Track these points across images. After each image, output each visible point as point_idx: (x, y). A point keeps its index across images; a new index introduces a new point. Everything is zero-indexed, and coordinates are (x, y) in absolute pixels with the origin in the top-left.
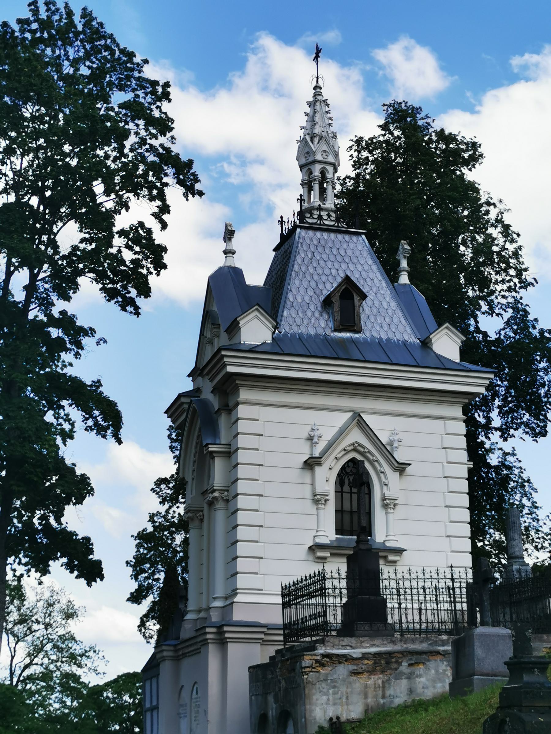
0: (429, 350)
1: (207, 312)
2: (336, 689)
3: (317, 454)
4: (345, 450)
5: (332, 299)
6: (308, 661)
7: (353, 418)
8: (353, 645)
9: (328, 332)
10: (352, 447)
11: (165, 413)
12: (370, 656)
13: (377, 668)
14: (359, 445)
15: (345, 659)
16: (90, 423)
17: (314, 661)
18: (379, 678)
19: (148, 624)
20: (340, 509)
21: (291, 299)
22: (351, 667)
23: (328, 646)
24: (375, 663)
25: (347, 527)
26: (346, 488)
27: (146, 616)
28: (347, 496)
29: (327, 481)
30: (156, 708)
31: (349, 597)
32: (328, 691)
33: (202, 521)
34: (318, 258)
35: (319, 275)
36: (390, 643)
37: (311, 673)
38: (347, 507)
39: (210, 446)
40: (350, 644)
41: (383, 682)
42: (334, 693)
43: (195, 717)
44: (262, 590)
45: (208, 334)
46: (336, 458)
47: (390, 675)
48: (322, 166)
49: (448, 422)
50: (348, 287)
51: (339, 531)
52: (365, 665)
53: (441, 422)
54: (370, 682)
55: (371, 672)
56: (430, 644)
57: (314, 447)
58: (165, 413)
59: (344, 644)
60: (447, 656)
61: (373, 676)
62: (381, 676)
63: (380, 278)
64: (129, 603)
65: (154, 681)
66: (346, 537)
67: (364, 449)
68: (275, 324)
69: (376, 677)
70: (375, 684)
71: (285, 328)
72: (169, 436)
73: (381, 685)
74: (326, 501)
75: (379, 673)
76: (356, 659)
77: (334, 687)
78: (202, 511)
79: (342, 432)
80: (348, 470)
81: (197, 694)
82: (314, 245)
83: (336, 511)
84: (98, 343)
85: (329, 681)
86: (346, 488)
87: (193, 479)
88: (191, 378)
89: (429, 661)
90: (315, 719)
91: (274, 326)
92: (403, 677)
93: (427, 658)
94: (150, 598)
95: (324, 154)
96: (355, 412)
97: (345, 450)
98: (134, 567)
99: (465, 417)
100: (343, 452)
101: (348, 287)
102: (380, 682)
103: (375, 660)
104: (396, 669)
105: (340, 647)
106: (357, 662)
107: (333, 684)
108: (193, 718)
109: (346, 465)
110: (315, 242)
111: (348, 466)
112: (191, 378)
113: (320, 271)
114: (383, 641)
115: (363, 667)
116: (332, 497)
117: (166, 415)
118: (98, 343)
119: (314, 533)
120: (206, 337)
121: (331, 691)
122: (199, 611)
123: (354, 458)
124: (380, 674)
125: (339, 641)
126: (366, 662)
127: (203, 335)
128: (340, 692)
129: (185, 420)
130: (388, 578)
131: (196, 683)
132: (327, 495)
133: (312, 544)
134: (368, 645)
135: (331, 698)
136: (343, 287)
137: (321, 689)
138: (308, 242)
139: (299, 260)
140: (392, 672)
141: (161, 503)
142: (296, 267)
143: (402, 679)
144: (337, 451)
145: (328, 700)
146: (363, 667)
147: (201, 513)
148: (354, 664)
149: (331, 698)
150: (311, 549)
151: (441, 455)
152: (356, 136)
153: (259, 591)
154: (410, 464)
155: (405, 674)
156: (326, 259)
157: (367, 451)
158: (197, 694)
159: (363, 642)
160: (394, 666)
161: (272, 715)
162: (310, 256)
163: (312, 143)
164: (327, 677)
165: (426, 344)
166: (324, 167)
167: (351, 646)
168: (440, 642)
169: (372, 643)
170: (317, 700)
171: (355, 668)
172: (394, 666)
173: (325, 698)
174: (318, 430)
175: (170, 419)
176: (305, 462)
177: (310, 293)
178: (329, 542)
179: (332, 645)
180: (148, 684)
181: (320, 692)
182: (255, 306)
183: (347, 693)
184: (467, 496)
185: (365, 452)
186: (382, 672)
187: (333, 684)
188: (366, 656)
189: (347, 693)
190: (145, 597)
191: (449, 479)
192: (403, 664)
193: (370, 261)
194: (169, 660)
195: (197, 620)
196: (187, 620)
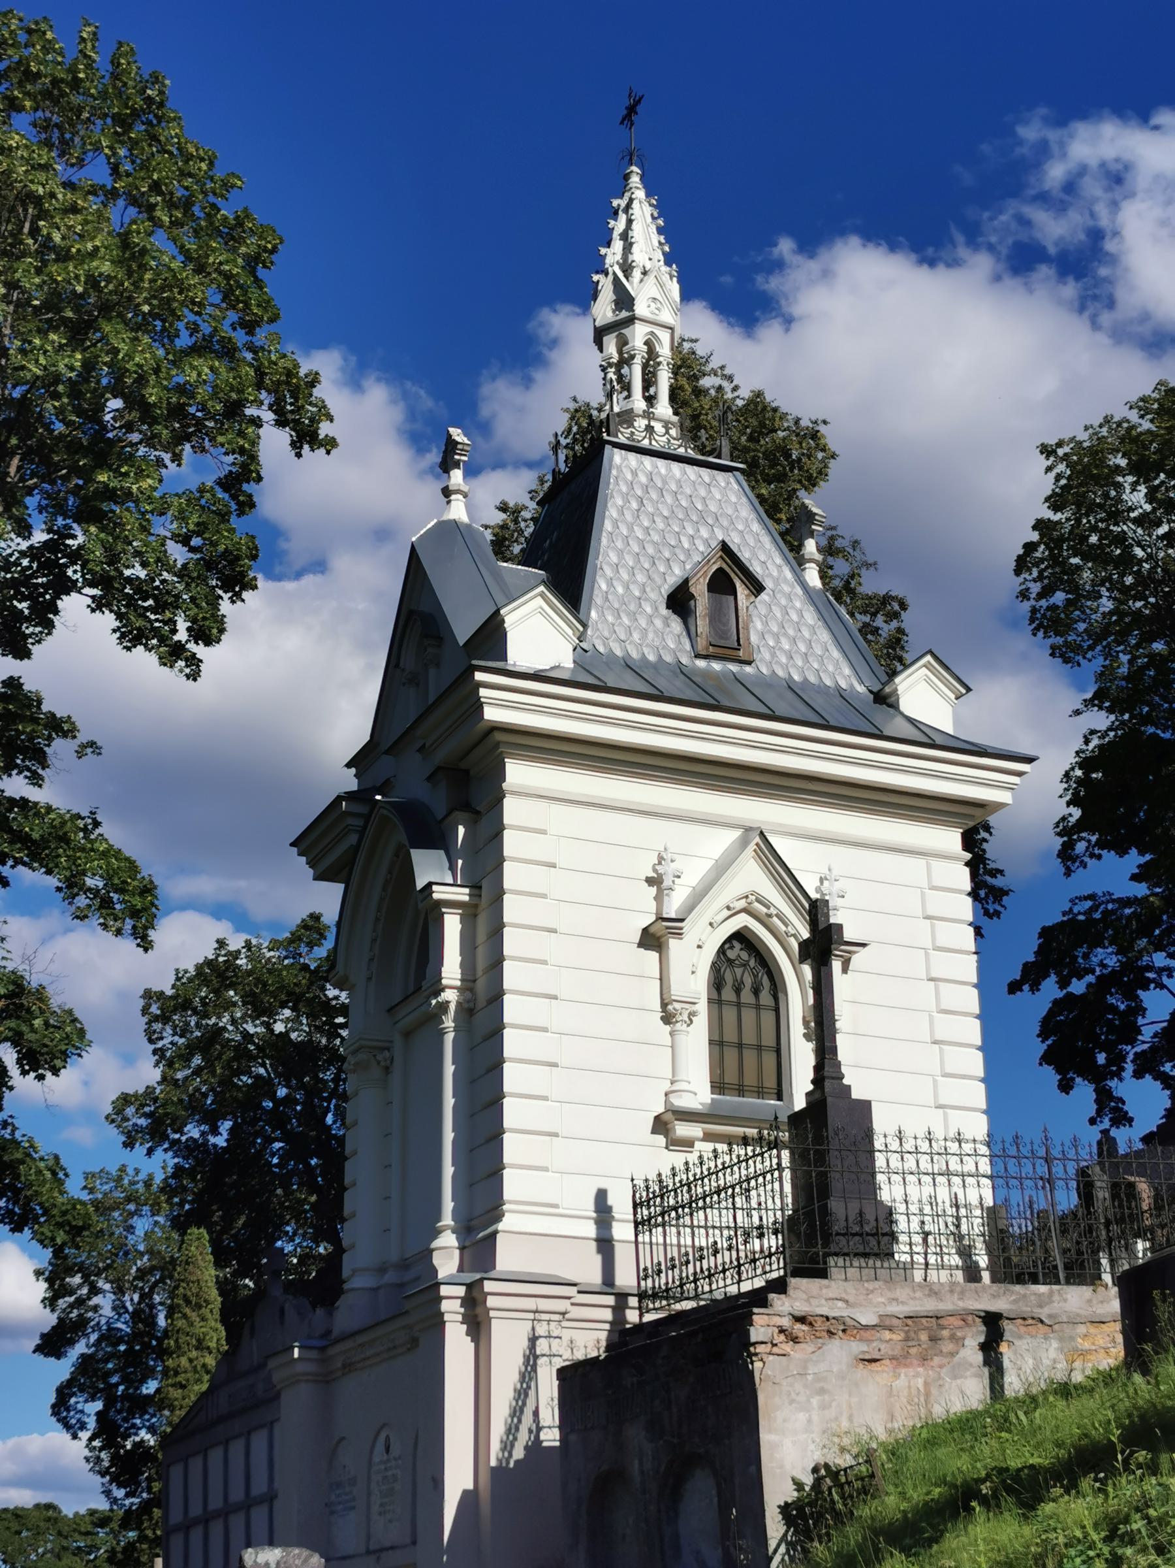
0: (891, 711)
1: (411, 613)
2: (826, 1397)
3: (671, 911)
4: (728, 908)
5: (692, 590)
6: (762, 1330)
7: (744, 843)
8: (851, 1299)
9: (685, 660)
10: (742, 904)
11: (292, 845)
12: (896, 1322)
13: (913, 1351)
14: (758, 900)
15: (842, 1327)
16: (82, 901)
17: (777, 1330)
18: (917, 1375)
19: (73, 1400)
20: (716, 1038)
21: (604, 587)
22: (857, 1347)
23: (796, 1299)
24: (907, 1339)
25: (731, 1077)
26: (728, 994)
27: (69, 1383)
28: (730, 1014)
29: (693, 972)
30: (270, 1498)
31: (793, 1210)
32: (809, 1401)
33: (387, 1070)
34: (651, 509)
35: (655, 543)
36: (929, 1296)
37: (771, 1358)
38: (730, 1035)
39: (435, 888)
40: (844, 1296)
41: (926, 1384)
42: (823, 1407)
43: (382, 1505)
44: (556, 1206)
45: (409, 661)
46: (711, 924)
47: (941, 1367)
48: (650, 330)
49: (936, 864)
50: (725, 566)
51: (718, 1086)
52: (887, 1342)
53: (921, 862)
54: (901, 1383)
55: (902, 1360)
56: (1015, 1302)
57: (666, 898)
58: (292, 845)
59: (831, 1295)
60: (1056, 1327)
61: (903, 1370)
62: (921, 1370)
63: (779, 560)
64: (39, 1358)
65: (259, 1441)
66: (728, 1098)
67: (768, 908)
68: (581, 629)
69: (911, 1372)
70: (909, 1387)
71: (596, 640)
72: (145, 1011)
73: (922, 1389)
74: (692, 1014)
75: (915, 1362)
76: (866, 1327)
77: (822, 1391)
78: (388, 1049)
79: (722, 868)
80: (731, 954)
81: (387, 1450)
82: (642, 485)
83: (711, 1042)
84: (80, 754)
85: (810, 1378)
86: (728, 994)
87: (369, 979)
88: (353, 770)
89: (1020, 1337)
90: (782, 1467)
91: (578, 634)
92: (968, 1373)
93: (1015, 1329)
94: (80, 1348)
95: (653, 305)
96: (748, 830)
97: (728, 908)
98: (50, 1281)
99: (968, 856)
100: (726, 913)
101: (725, 566)
102: (920, 1382)
103: (907, 1332)
104: (952, 1354)
105: (823, 1301)
106: (866, 1334)
107: (819, 1385)
108: (375, 1509)
109: (727, 946)
110: (643, 479)
111: (732, 947)
112: (353, 770)
113: (656, 537)
114: (914, 1292)
115: (882, 1347)
116: (702, 1007)
117: (295, 849)
118: (80, 754)
119: (666, 1086)
120: (403, 670)
121: (815, 1401)
122: (382, 1270)
123: (746, 927)
124: (919, 1365)
125: (821, 1289)
126: (887, 1335)
127: (397, 666)
128: (834, 1404)
129: (356, 849)
130: (913, 1150)
131: (384, 1426)
132: (694, 1003)
133: (662, 1110)
134: (883, 1300)
135: (815, 1418)
136: (715, 567)
137: (793, 1396)
138: (629, 477)
139: (612, 512)
140: (945, 1361)
141: (125, 1145)
142: (608, 525)
143: (966, 1378)
144: (712, 908)
145: (809, 1421)
146: (882, 1347)
147: (387, 1054)
148: (861, 1340)
149: (815, 1418)
150: (660, 1125)
151: (922, 932)
152: (575, 400)
153: (550, 1208)
154: (864, 945)
155: (971, 1365)
156: (666, 513)
157: (773, 911)
158: (387, 1450)
159: (872, 1292)
160: (948, 1347)
161: (642, 1472)
162: (634, 505)
163: (627, 278)
164: (806, 1368)
165: (884, 699)
166: (652, 333)
167: (846, 1302)
168: (1033, 1298)
169: (890, 1295)
170: (784, 1421)
171: (865, 1348)
172: (948, 1347)
173: (802, 1417)
174: (672, 861)
175: (304, 859)
176: (645, 931)
177: (641, 578)
178: (700, 1107)
179: (805, 1296)
180: (176, 1472)
181: (792, 1402)
182: (536, 586)
183: (850, 1407)
184: (978, 1022)
185: (770, 916)
186: (924, 1359)
187: (819, 1385)
188: (887, 1323)
189: (850, 1407)
190: (72, 1343)
191: (941, 984)
192: (967, 1342)
193: (756, 527)
194: (307, 1381)
195: (378, 1288)
196: (352, 1290)
